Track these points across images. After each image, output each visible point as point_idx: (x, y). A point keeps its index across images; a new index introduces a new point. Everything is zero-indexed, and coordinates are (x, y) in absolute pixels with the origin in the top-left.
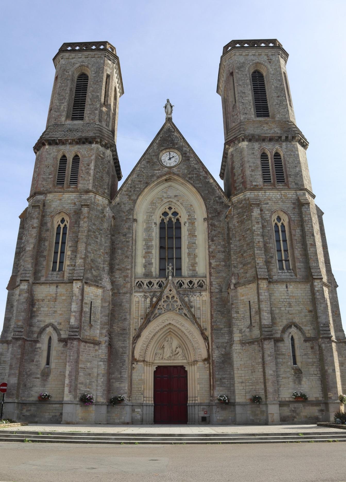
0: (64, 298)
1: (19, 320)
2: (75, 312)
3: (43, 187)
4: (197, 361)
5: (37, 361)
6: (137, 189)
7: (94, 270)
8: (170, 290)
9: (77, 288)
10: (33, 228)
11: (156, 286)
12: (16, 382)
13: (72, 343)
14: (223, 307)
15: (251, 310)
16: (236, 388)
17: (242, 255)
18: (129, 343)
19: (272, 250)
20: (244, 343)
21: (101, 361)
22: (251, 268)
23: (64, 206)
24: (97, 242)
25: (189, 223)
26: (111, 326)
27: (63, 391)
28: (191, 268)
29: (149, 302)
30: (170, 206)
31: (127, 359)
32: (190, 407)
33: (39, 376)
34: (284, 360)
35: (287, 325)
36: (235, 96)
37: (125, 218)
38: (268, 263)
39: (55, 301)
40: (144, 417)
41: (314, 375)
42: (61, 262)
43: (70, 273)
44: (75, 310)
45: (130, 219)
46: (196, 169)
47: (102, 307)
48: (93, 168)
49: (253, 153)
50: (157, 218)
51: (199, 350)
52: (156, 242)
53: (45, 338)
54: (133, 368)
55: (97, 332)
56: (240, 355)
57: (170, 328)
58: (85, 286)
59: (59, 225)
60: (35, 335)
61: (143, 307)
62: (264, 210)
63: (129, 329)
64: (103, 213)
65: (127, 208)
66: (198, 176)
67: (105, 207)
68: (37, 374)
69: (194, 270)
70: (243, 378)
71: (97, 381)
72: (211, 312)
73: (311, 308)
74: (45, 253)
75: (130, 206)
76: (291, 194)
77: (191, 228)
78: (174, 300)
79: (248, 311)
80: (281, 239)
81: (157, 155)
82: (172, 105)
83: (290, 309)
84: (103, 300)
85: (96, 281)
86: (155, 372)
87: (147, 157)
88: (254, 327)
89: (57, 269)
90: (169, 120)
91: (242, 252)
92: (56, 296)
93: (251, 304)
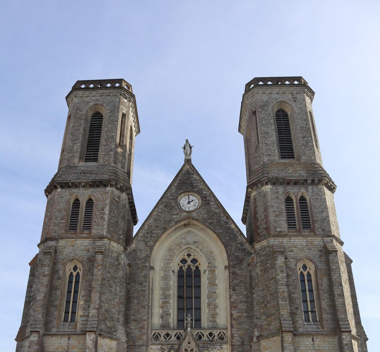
3: (55, 232)
6: (155, 235)
7: (109, 321)
8: (189, 343)
9: (91, 340)
17: (266, 305)
23: (77, 253)
24: (111, 291)
25: (209, 271)
28: (211, 319)
30: (189, 252)
37: (141, 266)
38: (293, 314)
42: (74, 313)
45: (146, 266)
46: (216, 214)
48: (107, 212)
49: (277, 197)
50: (175, 266)
52: (173, 292)
59: (72, 273)
62: (289, 258)
64: (118, 260)
65: (144, 255)
66: (219, 221)
67: (120, 254)
69: (215, 322)
75: (146, 253)
76: (318, 241)
80: (307, 289)
81: (176, 199)
82: (191, 145)
85: (110, 333)
87: (164, 201)
89: (69, 320)
90: (188, 161)
91: (265, 303)
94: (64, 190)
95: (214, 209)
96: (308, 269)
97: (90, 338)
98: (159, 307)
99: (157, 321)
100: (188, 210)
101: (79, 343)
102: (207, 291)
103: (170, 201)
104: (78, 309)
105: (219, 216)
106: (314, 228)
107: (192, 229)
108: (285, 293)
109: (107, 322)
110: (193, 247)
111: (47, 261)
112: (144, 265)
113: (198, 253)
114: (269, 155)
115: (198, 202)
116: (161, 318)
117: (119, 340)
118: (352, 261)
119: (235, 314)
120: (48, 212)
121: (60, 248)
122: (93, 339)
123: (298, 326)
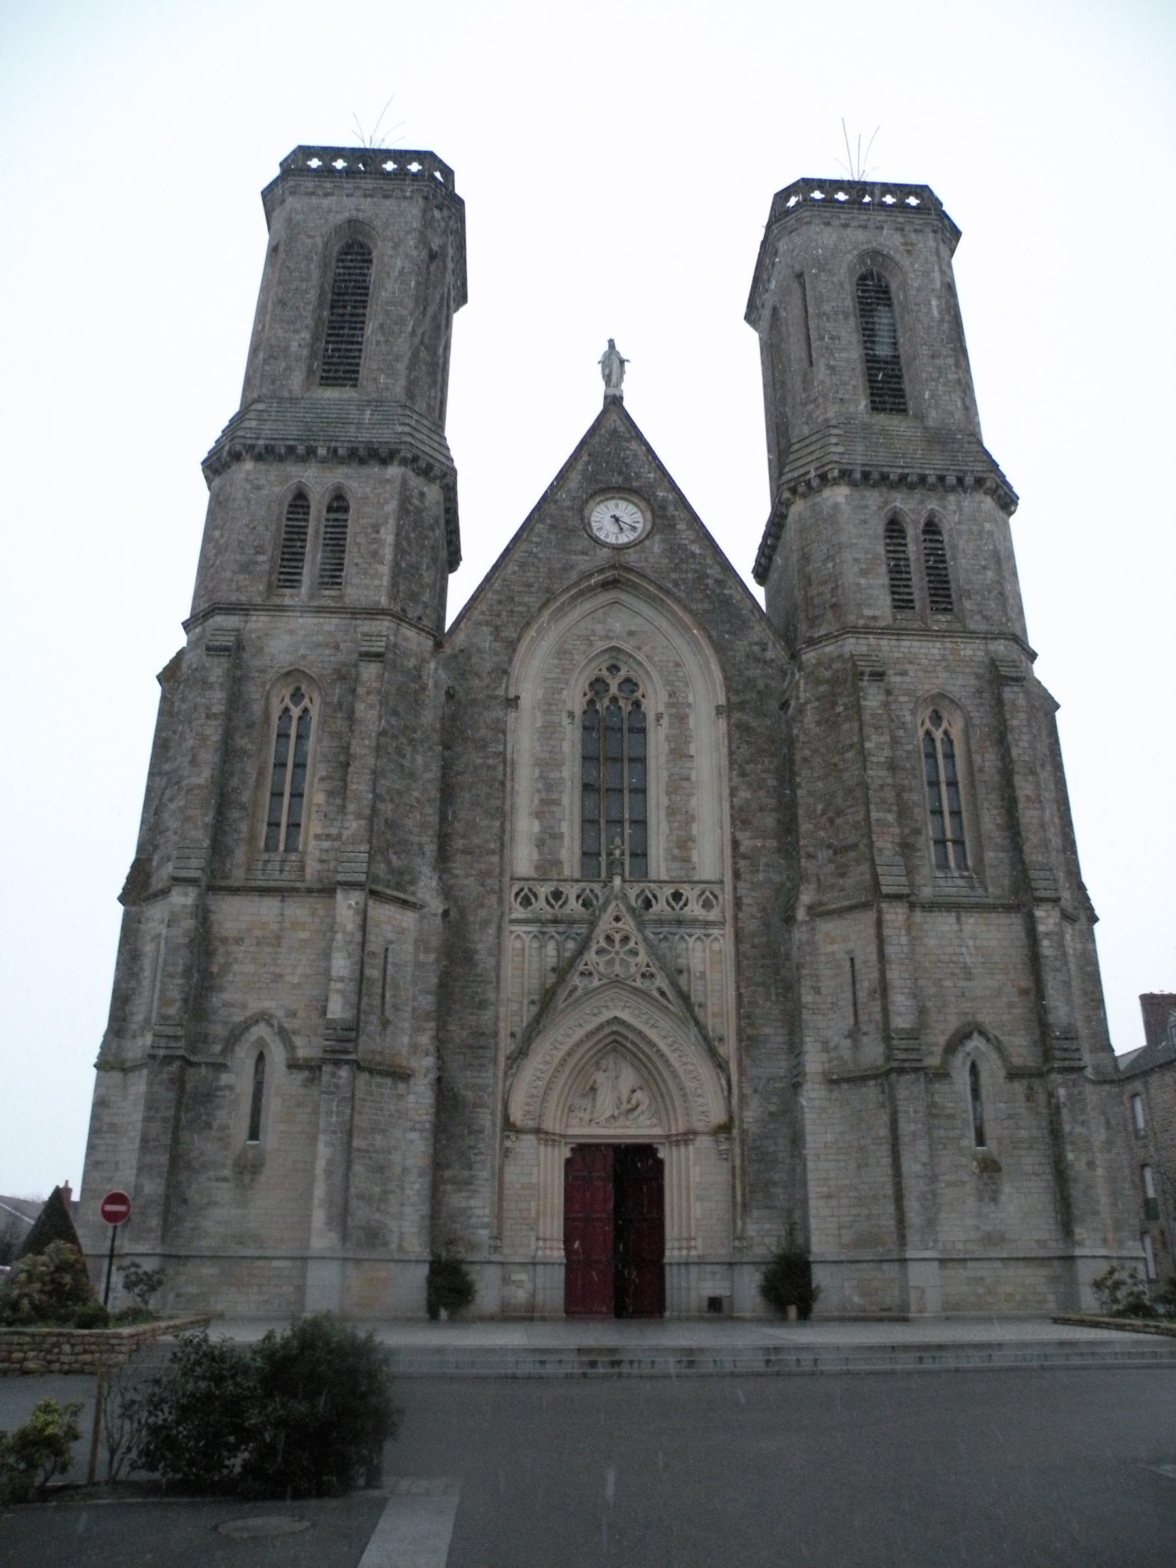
0: (304, 935)
1: (168, 1003)
2: (341, 979)
4: (695, 1133)
5: (223, 1128)
6: (520, 609)
7: (395, 853)
8: (617, 919)
10: (208, 717)
11: (574, 906)
12: (161, 1190)
13: (334, 1075)
14: (772, 969)
15: (858, 986)
16: (812, 1211)
17: (831, 821)
18: (495, 1075)
19: (917, 810)
20: (833, 1082)
21: (413, 1129)
22: (858, 862)
24: (402, 766)
26: (442, 1026)
27: (307, 1220)
28: (676, 852)
29: (554, 953)
30: (614, 662)
31: (487, 1120)
32: (675, 1268)
33: (227, 1172)
34: (951, 1134)
35: (957, 1031)
36: (809, 345)
37: (481, 696)
38: (906, 848)
39: (279, 946)
40: (540, 1298)
41: (1033, 1177)
42: (294, 826)
43: (322, 861)
44: (344, 973)
45: (496, 698)
47: (419, 965)
48: (390, 539)
49: (865, 522)
50: (575, 698)
51: (701, 1100)
52: (570, 773)
53: (244, 1057)
54: (506, 1152)
55: (409, 1041)
56: (824, 1116)
57: (613, 1033)
58: (370, 902)
59: (286, 710)
60: (217, 1048)
61: (535, 966)
62: (896, 692)
63: (495, 1034)
64: (420, 677)
65: (489, 666)
66: (702, 577)
67: (424, 661)
68: (223, 1165)
69: (687, 860)
70: (832, 1183)
71: (402, 1188)
72: (738, 988)
73: (1024, 984)
74: (245, 797)
76: (972, 650)
77: (677, 732)
78: (627, 948)
79: (848, 988)
80: (943, 777)
81: (581, 511)
82: (624, 356)
83: (967, 984)
84: (421, 943)
85: (399, 887)
86: (568, 1162)
88: (865, 1034)
89: (282, 847)
90: (614, 403)
91: (831, 814)
92: (281, 929)
93: (857, 967)
94: (262, 467)
95: (687, 542)
96: (945, 724)
97: (346, 906)
98: (531, 814)
99: (524, 859)
100: (614, 541)
101: (313, 914)
102: (665, 773)
103: (566, 512)
104: (309, 817)
105: (699, 563)
106: (962, 611)
107: (623, 597)
108: (887, 789)
109: (394, 858)
110: (625, 647)
111: (217, 670)
112: (490, 693)
113: (640, 664)
114: (841, 399)
115: (641, 520)
116: (537, 846)
117: (422, 907)
118: (1057, 706)
119: (747, 842)
120: (214, 529)
121: (254, 636)
122: (357, 903)
123: (919, 880)
